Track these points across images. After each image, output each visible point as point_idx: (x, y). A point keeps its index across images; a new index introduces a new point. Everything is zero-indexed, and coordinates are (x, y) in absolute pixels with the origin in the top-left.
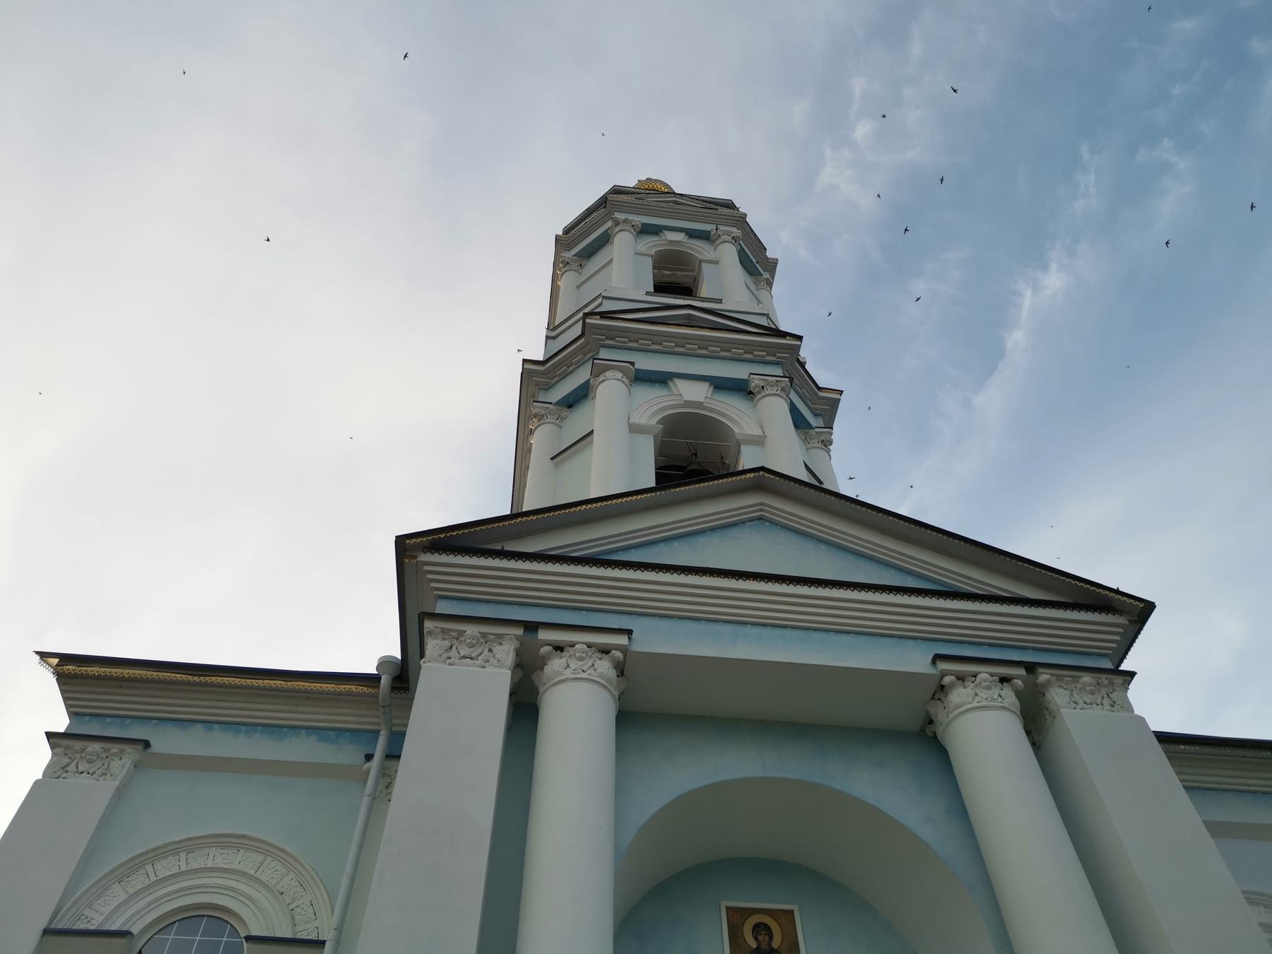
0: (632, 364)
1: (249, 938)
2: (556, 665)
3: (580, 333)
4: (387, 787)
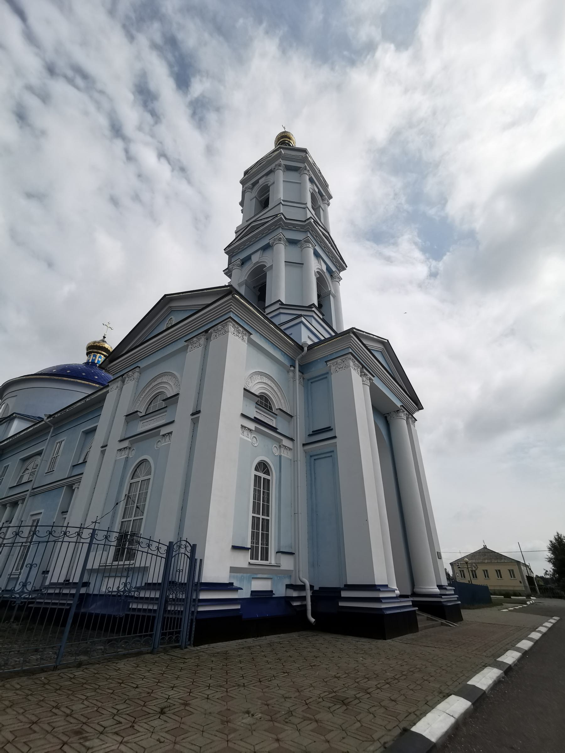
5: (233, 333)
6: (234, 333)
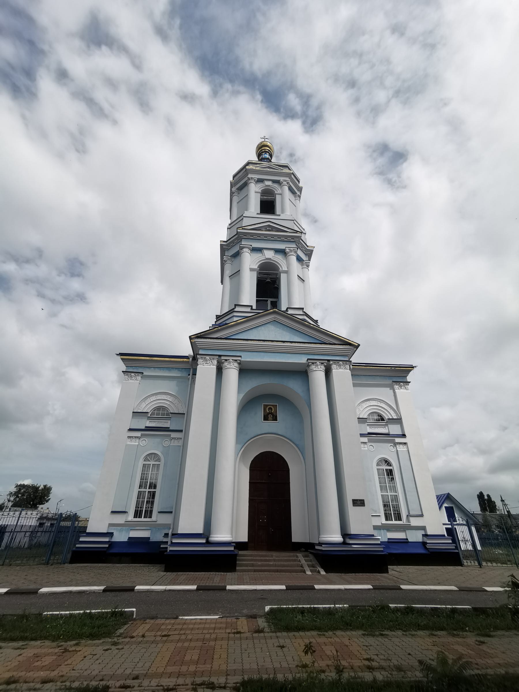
0: (251, 245)
1: (171, 413)
2: (226, 364)
3: (236, 233)
4: (193, 381)
5: (336, 369)
6: (337, 368)
